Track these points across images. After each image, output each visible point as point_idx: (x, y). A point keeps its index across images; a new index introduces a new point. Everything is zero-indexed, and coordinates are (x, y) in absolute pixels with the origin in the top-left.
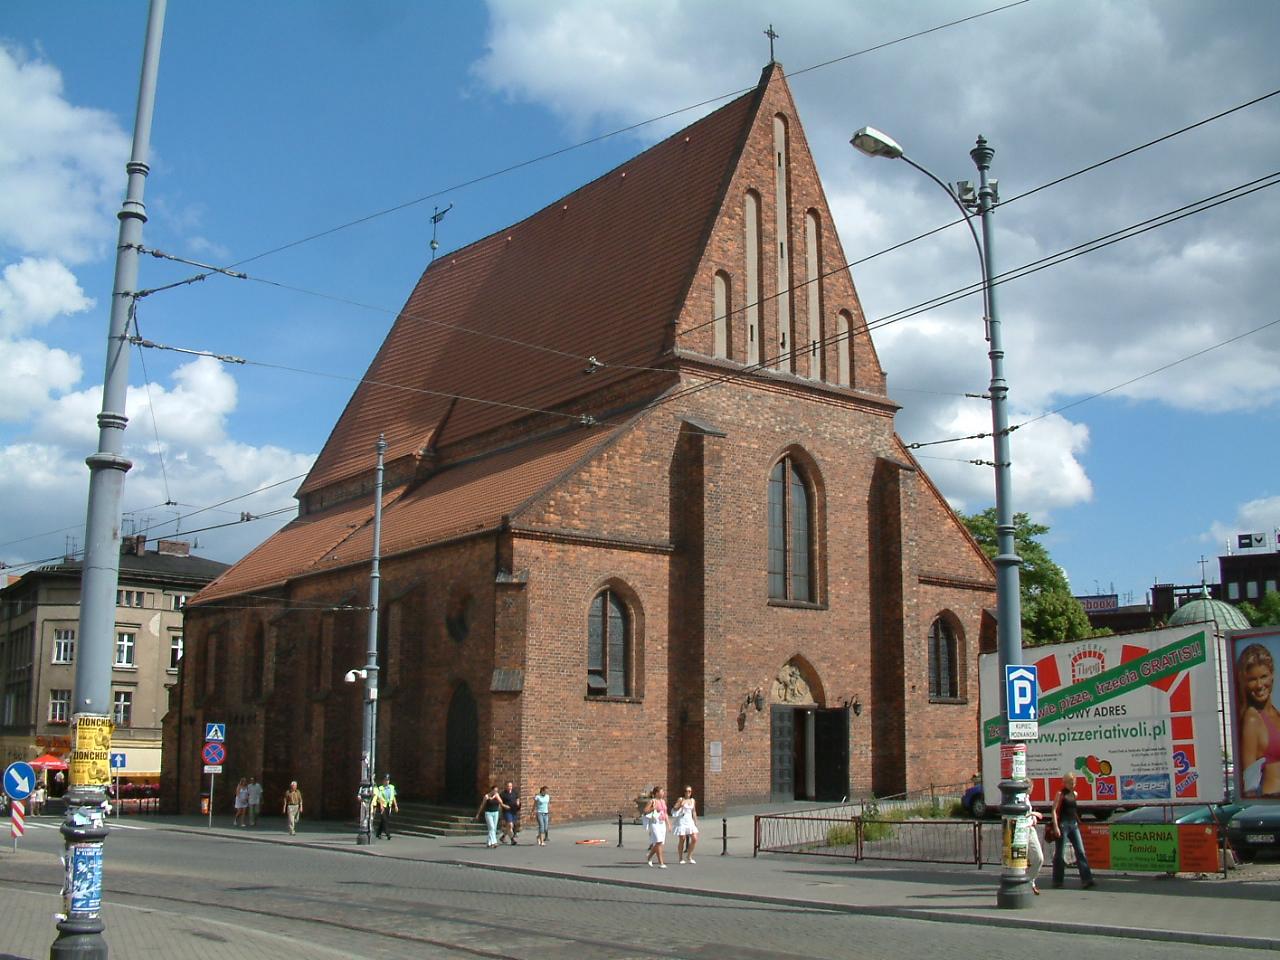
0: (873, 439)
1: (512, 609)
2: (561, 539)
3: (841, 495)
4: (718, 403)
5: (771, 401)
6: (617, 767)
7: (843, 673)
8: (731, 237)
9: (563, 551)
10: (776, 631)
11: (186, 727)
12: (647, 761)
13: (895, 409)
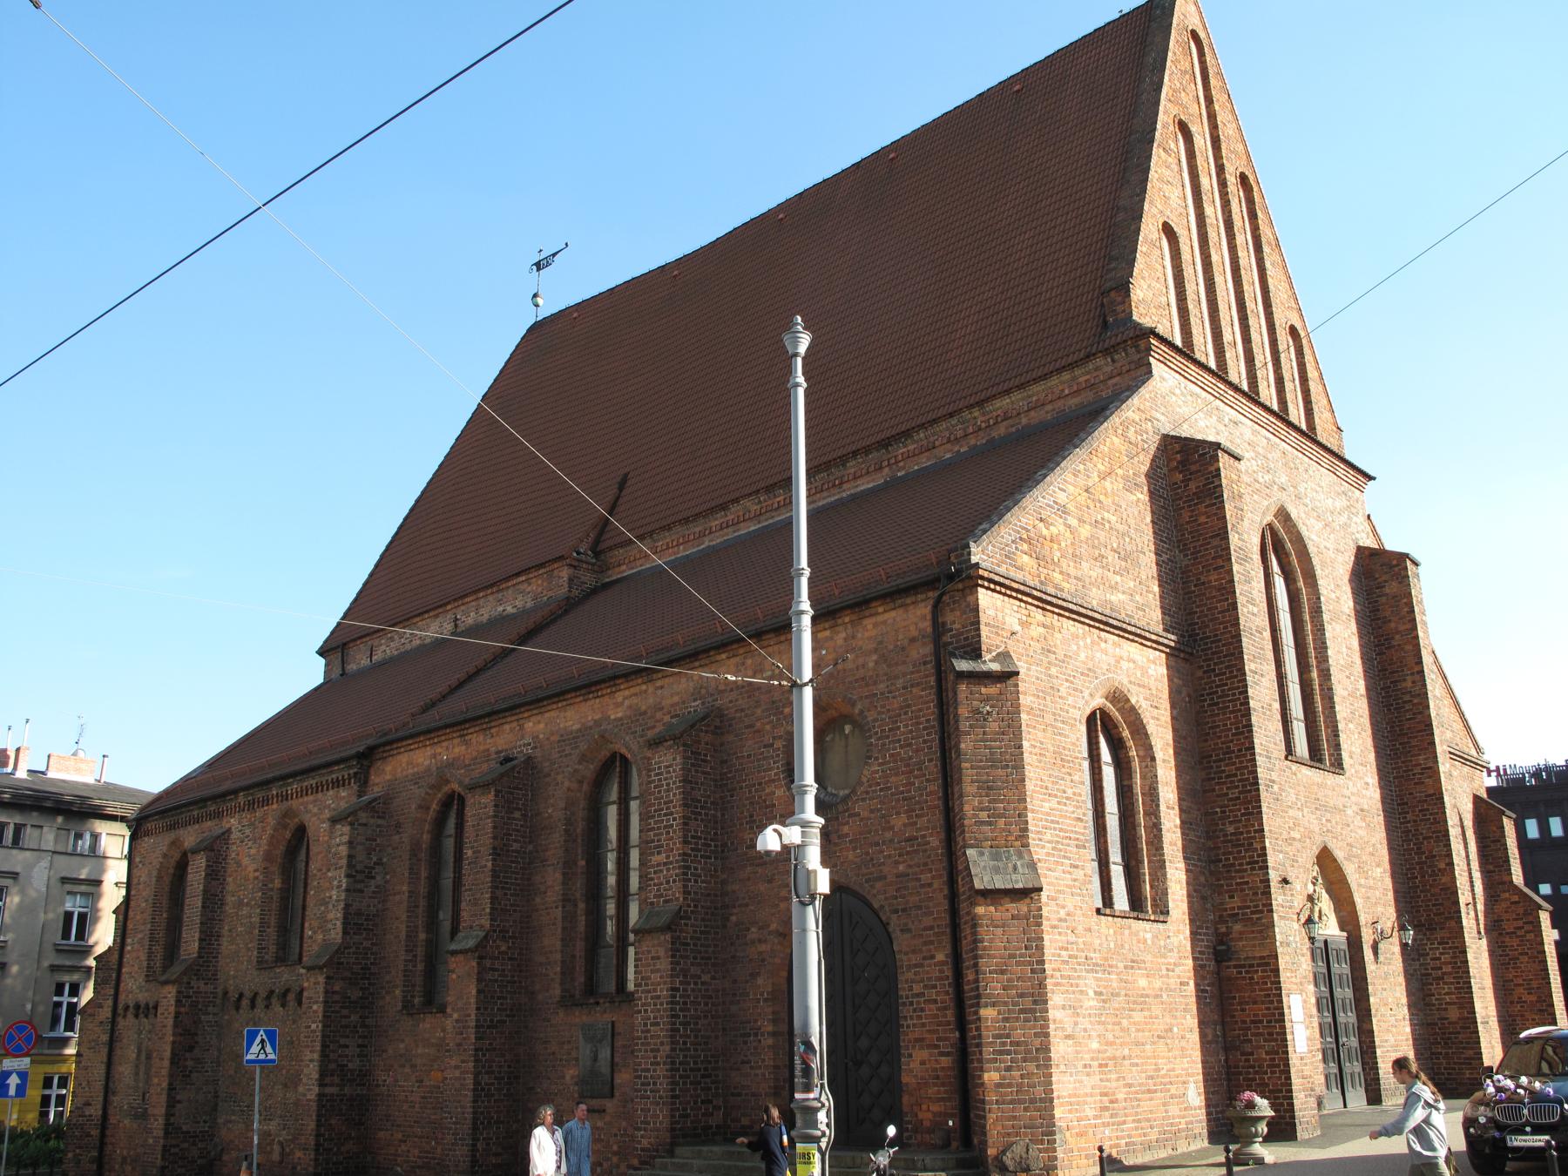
1: (993, 726)
9: (1044, 626)
11: (127, 1024)
13: (1370, 478)
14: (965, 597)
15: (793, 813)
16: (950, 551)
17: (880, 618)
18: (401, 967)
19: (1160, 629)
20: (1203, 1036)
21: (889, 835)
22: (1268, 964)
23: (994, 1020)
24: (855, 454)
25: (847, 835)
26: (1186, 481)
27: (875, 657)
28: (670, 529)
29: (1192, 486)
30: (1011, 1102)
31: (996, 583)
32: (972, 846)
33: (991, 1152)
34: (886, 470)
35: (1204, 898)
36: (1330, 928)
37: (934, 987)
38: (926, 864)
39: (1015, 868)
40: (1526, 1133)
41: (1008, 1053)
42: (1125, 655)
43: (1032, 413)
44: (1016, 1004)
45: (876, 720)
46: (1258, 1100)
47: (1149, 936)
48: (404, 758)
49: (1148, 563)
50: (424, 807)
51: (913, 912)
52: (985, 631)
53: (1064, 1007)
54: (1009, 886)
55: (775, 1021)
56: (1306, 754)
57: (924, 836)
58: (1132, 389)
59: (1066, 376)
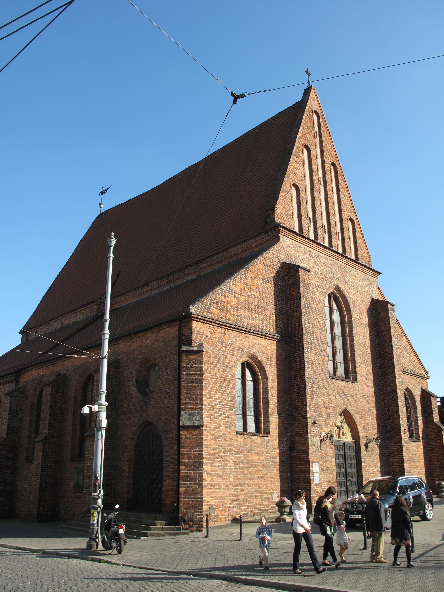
0: (369, 288)
1: (193, 369)
2: (221, 325)
3: (359, 318)
4: (299, 256)
5: (323, 260)
6: (256, 481)
7: (367, 422)
8: (298, 168)
9: (221, 333)
10: (334, 394)
12: (272, 477)
13: (380, 273)
14: (189, 324)
15: (98, 401)
16: (184, 308)
17: (165, 330)
18: (26, 446)
19: (274, 333)
20: (281, 477)
21: (163, 405)
22: (306, 452)
23: (185, 470)
24: (187, 266)
25: (152, 405)
26: (289, 279)
27: (163, 344)
28: (130, 292)
29: (291, 281)
30: (188, 498)
31: (200, 319)
32: (183, 410)
33: (180, 515)
34: (198, 272)
35: (286, 428)
36: (348, 438)
37: (173, 458)
38: (173, 416)
39: (196, 418)
40: (354, 514)
41: (189, 481)
42: (257, 342)
43: (243, 253)
44: (192, 465)
45: (162, 366)
46: (286, 500)
47: (259, 442)
48: (30, 373)
49: (271, 309)
50: (35, 391)
51: (169, 432)
52: (194, 336)
53: (218, 466)
54: (192, 425)
55: (129, 468)
56: (343, 375)
57: (173, 406)
58: (271, 246)
59: (253, 240)
